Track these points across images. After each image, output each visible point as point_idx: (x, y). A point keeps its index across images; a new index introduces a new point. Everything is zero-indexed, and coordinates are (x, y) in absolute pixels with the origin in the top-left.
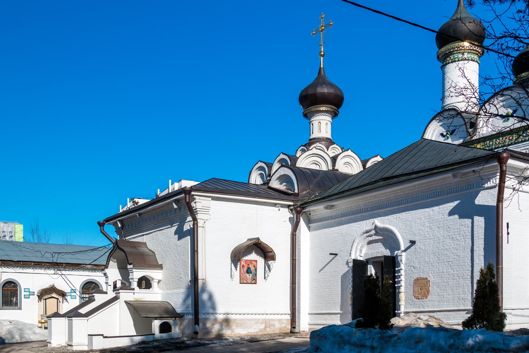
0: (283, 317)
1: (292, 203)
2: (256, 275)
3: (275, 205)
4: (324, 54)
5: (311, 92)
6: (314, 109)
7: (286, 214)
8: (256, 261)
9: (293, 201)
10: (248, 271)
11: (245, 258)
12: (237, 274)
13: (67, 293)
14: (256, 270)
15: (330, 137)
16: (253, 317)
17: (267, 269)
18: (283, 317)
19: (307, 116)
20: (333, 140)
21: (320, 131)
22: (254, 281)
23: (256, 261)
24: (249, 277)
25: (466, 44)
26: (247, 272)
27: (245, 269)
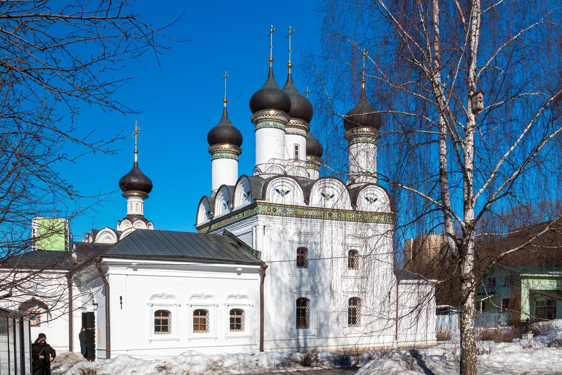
5: (127, 181)
6: (130, 194)
9: (68, 270)
15: (142, 214)
19: (126, 197)
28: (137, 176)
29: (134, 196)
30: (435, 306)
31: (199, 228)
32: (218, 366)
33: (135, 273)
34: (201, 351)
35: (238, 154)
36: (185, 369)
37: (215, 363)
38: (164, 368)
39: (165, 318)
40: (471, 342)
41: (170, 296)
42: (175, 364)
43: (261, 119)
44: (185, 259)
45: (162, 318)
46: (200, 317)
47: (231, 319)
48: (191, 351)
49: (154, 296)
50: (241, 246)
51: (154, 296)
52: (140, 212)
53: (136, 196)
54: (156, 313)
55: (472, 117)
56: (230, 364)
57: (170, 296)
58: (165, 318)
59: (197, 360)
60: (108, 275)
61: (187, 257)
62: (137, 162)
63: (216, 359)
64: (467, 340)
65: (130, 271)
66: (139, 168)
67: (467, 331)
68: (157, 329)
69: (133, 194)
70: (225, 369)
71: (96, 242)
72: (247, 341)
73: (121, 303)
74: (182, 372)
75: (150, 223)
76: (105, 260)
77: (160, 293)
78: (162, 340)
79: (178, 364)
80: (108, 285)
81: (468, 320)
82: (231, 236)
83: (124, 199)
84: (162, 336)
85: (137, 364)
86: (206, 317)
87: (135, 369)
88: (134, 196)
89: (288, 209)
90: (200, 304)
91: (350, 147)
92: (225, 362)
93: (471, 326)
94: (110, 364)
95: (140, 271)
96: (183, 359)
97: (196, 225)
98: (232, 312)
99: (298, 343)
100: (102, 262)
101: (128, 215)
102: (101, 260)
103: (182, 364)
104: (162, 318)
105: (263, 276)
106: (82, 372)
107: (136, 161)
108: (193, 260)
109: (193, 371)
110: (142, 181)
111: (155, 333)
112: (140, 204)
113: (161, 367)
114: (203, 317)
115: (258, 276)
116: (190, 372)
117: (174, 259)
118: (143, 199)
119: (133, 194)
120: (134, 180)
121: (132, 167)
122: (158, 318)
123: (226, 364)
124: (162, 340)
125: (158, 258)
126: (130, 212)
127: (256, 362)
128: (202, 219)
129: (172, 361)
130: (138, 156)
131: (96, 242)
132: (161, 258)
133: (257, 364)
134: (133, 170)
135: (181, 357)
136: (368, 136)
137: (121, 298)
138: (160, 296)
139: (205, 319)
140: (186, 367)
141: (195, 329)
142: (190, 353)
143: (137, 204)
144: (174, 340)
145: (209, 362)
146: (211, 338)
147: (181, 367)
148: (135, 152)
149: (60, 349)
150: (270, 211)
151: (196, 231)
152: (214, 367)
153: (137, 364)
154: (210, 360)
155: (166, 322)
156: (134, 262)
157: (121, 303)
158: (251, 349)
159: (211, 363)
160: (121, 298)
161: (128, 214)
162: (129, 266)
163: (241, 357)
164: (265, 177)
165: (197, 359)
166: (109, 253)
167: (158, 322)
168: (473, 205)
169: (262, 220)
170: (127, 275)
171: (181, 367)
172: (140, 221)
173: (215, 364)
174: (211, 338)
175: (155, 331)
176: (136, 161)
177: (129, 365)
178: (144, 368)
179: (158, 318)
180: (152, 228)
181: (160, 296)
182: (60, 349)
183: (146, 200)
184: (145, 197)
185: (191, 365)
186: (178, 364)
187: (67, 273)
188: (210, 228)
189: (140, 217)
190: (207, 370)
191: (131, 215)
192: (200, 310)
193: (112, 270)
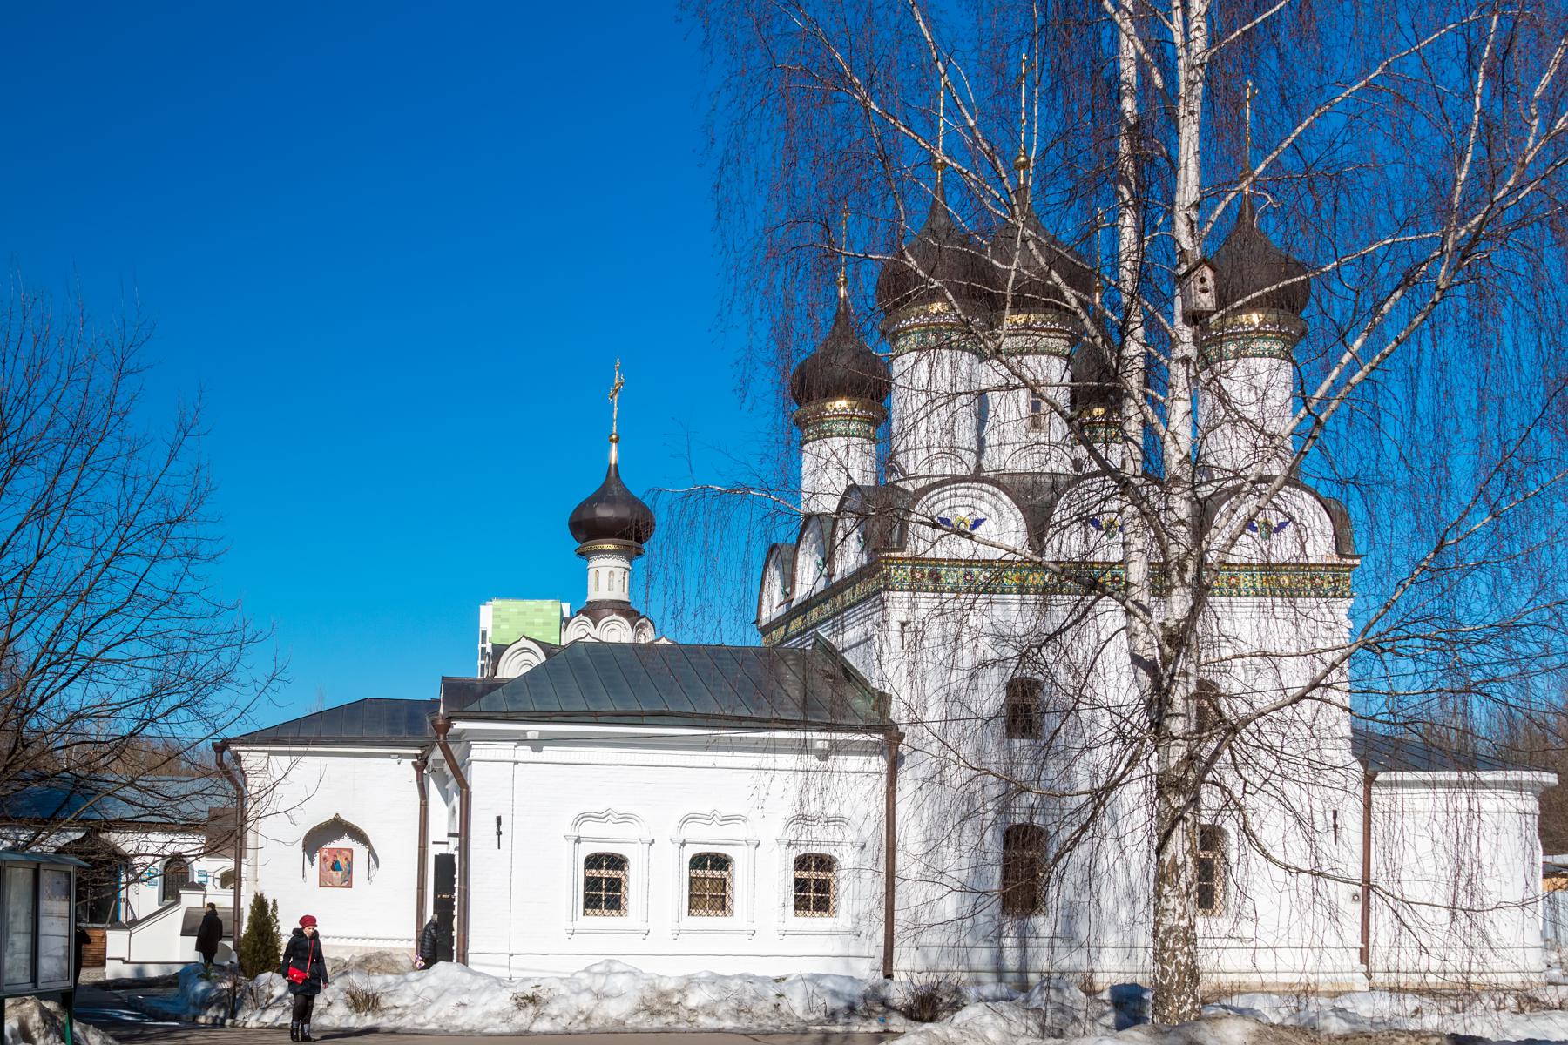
0: (404, 945)
1: (418, 752)
2: (350, 872)
3: (388, 756)
4: (618, 438)
5: (586, 515)
6: (593, 548)
7: (407, 769)
8: (351, 851)
9: (421, 748)
10: (335, 866)
11: (328, 846)
12: (314, 871)
13: (383, 998)
14: (350, 864)
15: (625, 597)
16: (343, 942)
17: (372, 862)
18: (404, 945)
19: (585, 555)
20: (633, 606)
21: (597, 589)
22: (347, 882)
23: (351, 851)
24: (337, 876)
25: (841, 404)
26: (333, 868)
27: (329, 863)
28: (611, 502)
29: (604, 552)
30: (1540, 858)
31: (765, 631)
32: (669, 1004)
33: (537, 756)
34: (634, 962)
35: (874, 422)
36: (584, 1007)
37: (663, 995)
38: (533, 1000)
39: (822, 875)
40: (1178, 964)
41: (624, 818)
42: (563, 991)
43: (905, 328)
44: (666, 720)
45: (813, 874)
46: (708, 873)
47: (798, 881)
48: (610, 961)
49: (583, 818)
50: (849, 680)
51: (583, 818)
52: (620, 594)
53: (609, 552)
54: (587, 860)
55: (1186, 334)
56: (703, 1002)
57: (624, 818)
58: (822, 875)
59: (619, 985)
60: (470, 763)
61: (672, 714)
62: (616, 465)
63: (668, 986)
64: (1166, 957)
65: (525, 752)
66: (620, 481)
67: (1165, 932)
68: (591, 903)
69: (600, 547)
70: (686, 1013)
71: (498, 676)
72: (835, 946)
73: (499, 833)
74: (574, 1013)
75: (644, 620)
76: (459, 725)
77: (600, 809)
78: (602, 932)
79: (568, 994)
80: (467, 788)
81: (1168, 901)
82: (831, 652)
83: (582, 561)
84: (603, 921)
85: (474, 987)
86: (830, 875)
87: (465, 999)
88: (604, 552)
89: (943, 571)
90: (709, 838)
91: (805, 447)
92: (690, 996)
93: (1182, 917)
94: (414, 984)
95: (549, 753)
96: (586, 980)
97: (757, 621)
98: (802, 863)
99: (998, 959)
100: (451, 731)
101: (589, 603)
102: (450, 726)
103: (578, 994)
104: (813, 874)
105: (895, 763)
106: (349, 999)
107: (613, 462)
108: (703, 722)
109: (601, 1012)
110: (623, 512)
111: (796, 915)
112: (619, 574)
113: (527, 998)
114: (717, 874)
115: (878, 763)
116: (594, 1015)
117: (638, 720)
118: (630, 560)
119: (600, 547)
120: (604, 512)
121: (602, 479)
122: (595, 873)
123: (692, 1001)
124: (602, 932)
125: (593, 719)
126: (593, 595)
127: (775, 1001)
128: (772, 608)
129: (556, 984)
130: (619, 451)
131: (498, 676)
132: (602, 719)
133: (777, 1006)
134: (605, 488)
135: (584, 975)
136: (850, 418)
137: (499, 820)
138: (602, 817)
139: (723, 881)
140: (586, 1002)
141: (692, 906)
142: (607, 966)
143: (611, 573)
144: (634, 932)
145: (647, 994)
146: (739, 932)
147: (574, 1000)
148: (612, 440)
149: (336, 942)
150: (919, 581)
151: (755, 640)
152: (658, 1007)
153: (474, 987)
154: (653, 988)
155: (823, 886)
156: (533, 730)
157: (499, 833)
158: (848, 966)
159: (654, 995)
160: (499, 820)
161: (589, 599)
162: (521, 740)
163: (735, 985)
164: (909, 486)
165: (620, 982)
166: (474, 707)
167: (596, 883)
168: (1188, 577)
169: (899, 606)
170: (516, 763)
171: (574, 1000)
172: (615, 616)
173: (664, 1000)
174: (739, 932)
175: (796, 908)
176: (613, 462)
177: (454, 989)
178: (485, 998)
179: (595, 873)
180: (648, 636)
181: (602, 817)
182: (336, 942)
183: (638, 562)
184: (631, 554)
185: (600, 996)
186: (568, 994)
187: (417, 756)
188: (786, 630)
189: (616, 605)
190: (637, 1012)
191: (595, 602)
192: (709, 854)
193: (478, 751)
